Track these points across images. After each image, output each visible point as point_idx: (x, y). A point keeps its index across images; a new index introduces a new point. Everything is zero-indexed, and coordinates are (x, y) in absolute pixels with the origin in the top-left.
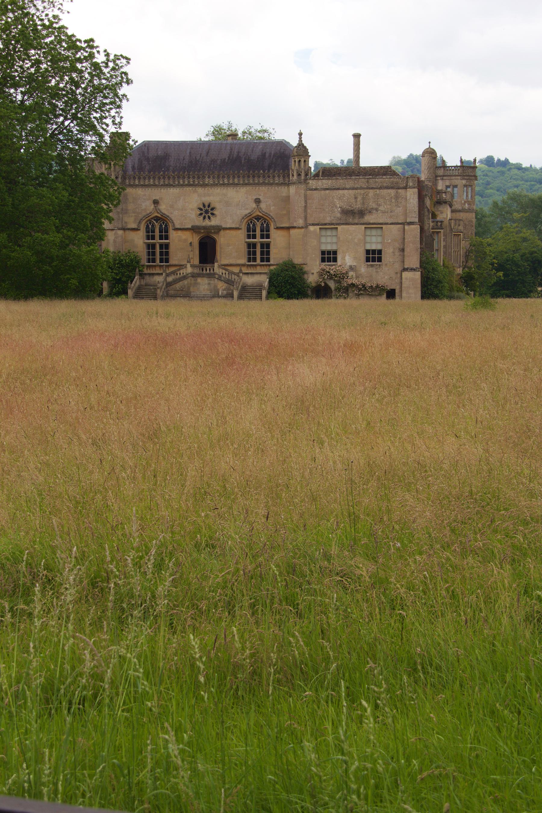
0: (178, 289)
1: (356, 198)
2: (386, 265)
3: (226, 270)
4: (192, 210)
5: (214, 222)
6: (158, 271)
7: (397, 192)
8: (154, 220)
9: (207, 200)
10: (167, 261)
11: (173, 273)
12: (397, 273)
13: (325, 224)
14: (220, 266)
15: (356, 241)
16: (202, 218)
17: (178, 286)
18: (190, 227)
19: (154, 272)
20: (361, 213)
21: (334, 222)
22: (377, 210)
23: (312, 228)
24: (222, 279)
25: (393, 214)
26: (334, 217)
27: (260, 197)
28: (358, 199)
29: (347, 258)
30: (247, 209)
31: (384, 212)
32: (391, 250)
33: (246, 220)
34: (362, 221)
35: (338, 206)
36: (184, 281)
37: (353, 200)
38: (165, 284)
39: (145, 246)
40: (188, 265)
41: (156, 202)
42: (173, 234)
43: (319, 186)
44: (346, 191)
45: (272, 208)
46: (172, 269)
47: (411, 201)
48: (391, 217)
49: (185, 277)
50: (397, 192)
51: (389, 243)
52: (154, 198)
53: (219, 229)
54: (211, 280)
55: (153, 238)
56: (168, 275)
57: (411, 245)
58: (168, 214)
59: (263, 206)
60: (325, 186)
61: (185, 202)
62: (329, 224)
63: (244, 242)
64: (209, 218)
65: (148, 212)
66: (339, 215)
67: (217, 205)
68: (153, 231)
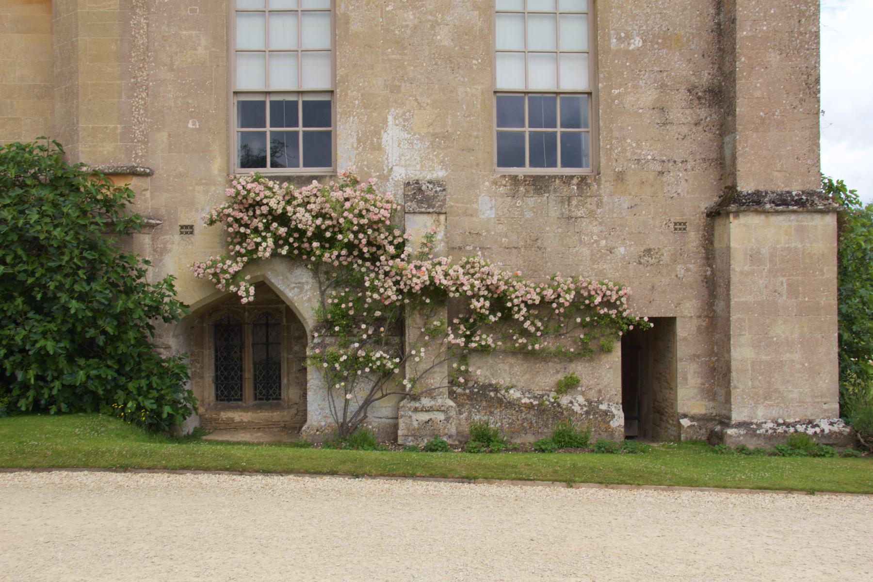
2: (620, 177)
12: (680, 227)
15: (444, 37)
32: (648, 96)
51: (634, 56)
57: (773, 57)
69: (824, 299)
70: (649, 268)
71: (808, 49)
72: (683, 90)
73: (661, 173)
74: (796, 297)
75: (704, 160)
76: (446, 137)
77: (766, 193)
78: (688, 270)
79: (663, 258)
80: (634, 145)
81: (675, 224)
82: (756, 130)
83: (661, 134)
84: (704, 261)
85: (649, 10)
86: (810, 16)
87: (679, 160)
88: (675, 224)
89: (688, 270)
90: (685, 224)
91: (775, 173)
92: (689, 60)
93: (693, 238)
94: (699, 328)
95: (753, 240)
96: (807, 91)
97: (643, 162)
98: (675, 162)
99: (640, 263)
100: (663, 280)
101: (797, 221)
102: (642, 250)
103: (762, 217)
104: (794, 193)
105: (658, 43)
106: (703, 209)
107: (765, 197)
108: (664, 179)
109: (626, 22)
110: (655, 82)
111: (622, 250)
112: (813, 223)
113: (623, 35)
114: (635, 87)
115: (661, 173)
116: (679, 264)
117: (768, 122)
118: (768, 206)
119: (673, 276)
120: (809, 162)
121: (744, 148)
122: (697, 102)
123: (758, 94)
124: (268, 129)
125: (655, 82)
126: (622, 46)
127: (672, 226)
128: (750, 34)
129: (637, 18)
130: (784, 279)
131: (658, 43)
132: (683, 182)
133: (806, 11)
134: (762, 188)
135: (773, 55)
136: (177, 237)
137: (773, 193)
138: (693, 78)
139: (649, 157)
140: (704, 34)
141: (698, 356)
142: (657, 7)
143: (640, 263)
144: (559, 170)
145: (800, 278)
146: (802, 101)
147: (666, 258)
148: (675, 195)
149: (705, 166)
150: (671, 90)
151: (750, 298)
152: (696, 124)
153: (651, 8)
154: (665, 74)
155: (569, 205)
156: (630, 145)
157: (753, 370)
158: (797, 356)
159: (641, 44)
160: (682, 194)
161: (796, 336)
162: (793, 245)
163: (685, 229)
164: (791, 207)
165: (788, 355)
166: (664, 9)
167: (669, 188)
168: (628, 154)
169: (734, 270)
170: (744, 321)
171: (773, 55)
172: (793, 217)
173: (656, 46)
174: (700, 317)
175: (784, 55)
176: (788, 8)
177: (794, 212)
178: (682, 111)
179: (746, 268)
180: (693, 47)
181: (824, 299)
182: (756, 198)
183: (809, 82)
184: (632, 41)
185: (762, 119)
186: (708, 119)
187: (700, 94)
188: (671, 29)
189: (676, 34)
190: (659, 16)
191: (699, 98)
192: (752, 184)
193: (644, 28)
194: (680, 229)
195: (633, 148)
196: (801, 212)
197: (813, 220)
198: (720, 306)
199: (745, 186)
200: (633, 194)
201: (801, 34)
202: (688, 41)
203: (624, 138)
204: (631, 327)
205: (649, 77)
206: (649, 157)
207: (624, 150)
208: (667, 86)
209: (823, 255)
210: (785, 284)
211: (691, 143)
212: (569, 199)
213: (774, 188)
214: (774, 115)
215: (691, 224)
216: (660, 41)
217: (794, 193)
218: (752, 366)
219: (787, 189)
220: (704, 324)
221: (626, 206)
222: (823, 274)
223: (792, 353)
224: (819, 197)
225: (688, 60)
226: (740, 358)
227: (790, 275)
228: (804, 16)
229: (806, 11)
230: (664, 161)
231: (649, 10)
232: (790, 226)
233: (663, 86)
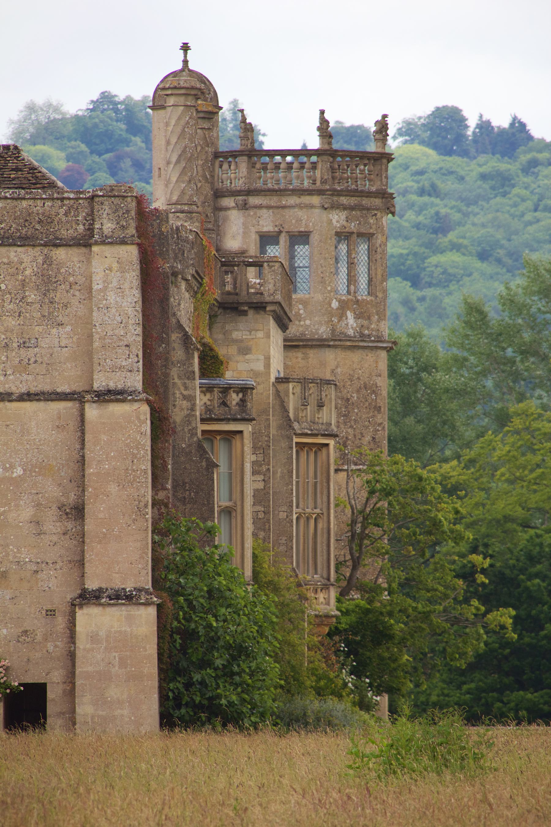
7: (48, 261)
12: (51, 613)
25: (31, 352)
47: (112, 297)
50: (48, 261)
57: (113, 488)
69: (146, 669)
70: (25, 645)
71: (139, 482)
72: (54, 507)
73: (36, 572)
74: (126, 668)
75: (70, 562)
77: (107, 589)
78: (56, 646)
79: (36, 637)
80: (15, 550)
81: (47, 611)
82: (100, 542)
83: (36, 542)
84: (69, 640)
85: (28, 446)
86: (141, 458)
87: (50, 562)
88: (47, 611)
89: (56, 646)
90: (54, 611)
91: (114, 575)
92: (60, 485)
93: (61, 622)
94: (64, 691)
95: (94, 625)
96: (138, 513)
97: (22, 563)
98: (47, 563)
99: (19, 641)
100: (37, 654)
101: (127, 611)
102: (21, 631)
103: (101, 608)
104: (127, 590)
105: (35, 472)
106: (68, 600)
107: (104, 593)
108: (39, 577)
109: (11, 456)
110: (33, 501)
112: (139, 613)
113: (8, 466)
114: (17, 506)
115: (36, 572)
116: (49, 642)
117: (108, 536)
118: (103, 600)
119: (44, 651)
120: (140, 566)
121: (90, 555)
122: (65, 517)
123: (101, 516)
125: (33, 501)
126: (7, 474)
127: (44, 612)
128: (96, 471)
129: (20, 452)
130: (116, 654)
131: (35, 472)
132: (53, 578)
133: (137, 454)
134: (104, 586)
135: (113, 487)
137: (111, 589)
138: (62, 498)
139: (27, 560)
140: (72, 464)
141: (63, 714)
142: (34, 444)
143: (19, 641)
145: (128, 653)
146: (134, 520)
147: (39, 638)
148: (47, 589)
149: (70, 566)
150: (45, 508)
151: (90, 669)
152: (64, 534)
153: (30, 445)
154: (40, 495)
155: (164, 800)
156: (12, 550)
157: (93, 722)
158: (125, 712)
159: (22, 472)
160: (52, 588)
161: (125, 696)
162: (123, 629)
163: (54, 615)
164: (120, 601)
165: (119, 711)
166: (41, 445)
167: (42, 583)
168: (11, 558)
169: (79, 648)
170: (86, 686)
171: (113, 487)
172: (124, 608)
173: (34, 474)
174: (65, 683)
175: (121, 486)
176: (124, 452)
177: (123, 604)
178: (53, 524)
179: (88, 646)
180: (63, 474)
181: (146, 669)
182: (97, 594)
183: (140, 506)
184: (15, 470)
185: (105, 534)
186: (74, 530)
187: (68, 510)
188: (46, 461)
189: (49, 465)
190: (36, 450)
191: (67, 514)
192: (96, 583)
193: (25, 460)
194: (51, 615)
195: (14, 552)
196: (129, 604)
197: (138, 610)
199: (92, 585)
200: (14, 588)
201: (134, 471)
202: (59, 469)
203: (8, 545)
204: (8, 691)
205: (28, 498)
206: (27, 560)
207: (7, 555)
208: (42, 504)
209: (146, 636)
210: (117, 658)
211: (60, 548)
213: (113, 586)
214: (113, 531)
215: (59, 611)
216: (37, 470)
217: (127, 590)
218: (92, 719)
219: (123, 586)
220: (68, 688)
221: (8, 597)
222: (146, 650)
223: (122, 709)
224: (146, 593)
225: (58, 485)
226: (83, 713)
227: (121, 651)
228: (136, 457)
229: (137, 454)
230: (38, 563)
231: (28, 446)
232: (121, 615)
233: (38, 505)
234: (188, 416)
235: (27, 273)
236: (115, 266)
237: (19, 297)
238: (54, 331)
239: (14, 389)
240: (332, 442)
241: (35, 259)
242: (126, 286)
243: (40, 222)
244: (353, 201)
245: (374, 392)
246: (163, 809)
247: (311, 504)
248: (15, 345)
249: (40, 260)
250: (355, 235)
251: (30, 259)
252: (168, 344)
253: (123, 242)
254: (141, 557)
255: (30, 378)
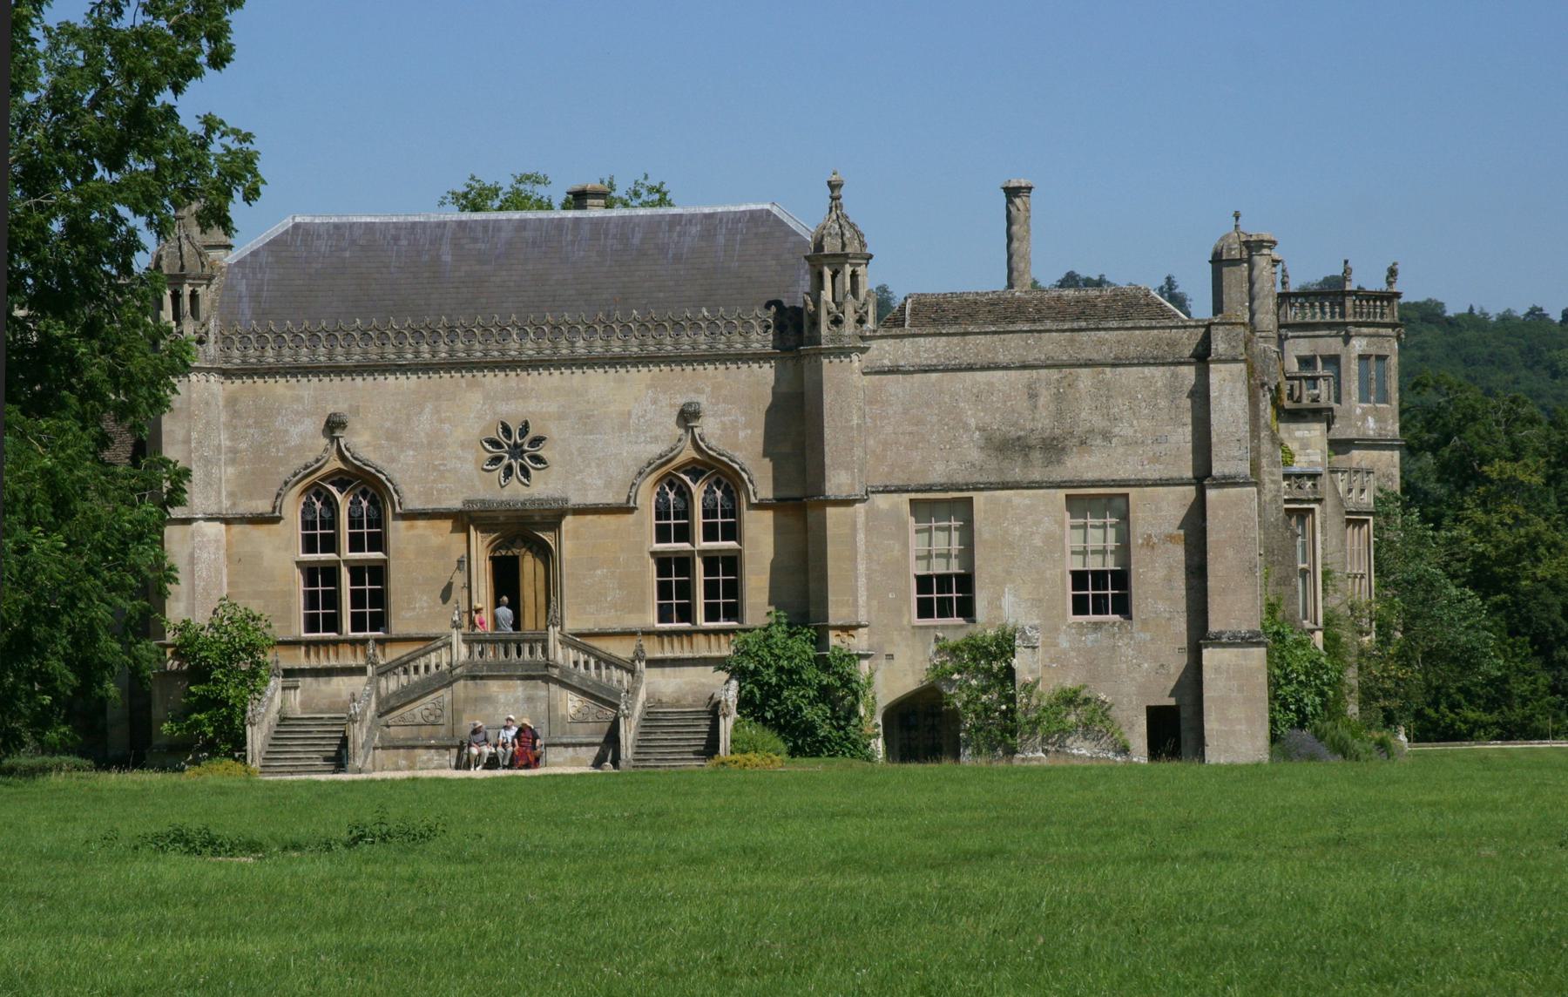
0: (419, 719)
1: (1033, 396)
3: (589, 651)
4: (463, 445)
5: (543, 487)
6: (348, 658)
7: (1175, 376)
8: (333, 484)
9: (513, 411)
10: (379, 622)
11: (403, 665)
13: (930, 489)
14: (569, 641)
15: (1038, 541)
16: (499, 471)
17: (419, 709)
18: (456, 504)
19: (333, 662)
20: (1054, 447)
21: (959, 479)
22: (1106, 436)
23: (882, 502)
24: (575, 681)
25: (1162, 448)
26: (960, 464)
27: (703, 400)
28: (1042, 401)
29: (1008, 600)
30: (655, 439)
31: (1130, 443)
33: (654, 477)
34: (1057, 474)
35: (972, 422)
36: (441, 692)
37: (1023, 404)
38: (373, 705)
39: (299, 577)
40: (456, 637)
41: (333, 426)
42: (398, 531)
43: (904, 356)
44: (1000, 373)
45: (742, 434)
46: (395, 653)
47: (1226, 402)
48: (1156, 459)
49: (446, 679)
50: (1175, 376)
52: (331, 409)
53: (554, 516)
54: (536, 687)
55: (330, 544)
56: (384, 672)
57: (1230, 553)
58: (379, 463)
59: (710, 428)
60: (925, 359)
61: (441, 421)
62: (945, 489)
63: (647, 556)
64: (525, 471)
65: (311, 457)
66: (975, 455)
67: (552, 430)
68: (686, 513)
76: (1040, 600)
82: (1219, 595)
111: (1146, 665)
115: (1169, 619)
124: (365, 530)
130: (1235, 683)
136: (884, 661)
144: (368, 634)
149: (1009, 630)
198: (1131, 483)
212: (1114, 635)
213: (1231, 629)
234: (1276, 496)
235: (1159, 384)
236: (1228, 377)
237: (1152, 404)
238: (1180, 430)
239: (1149, 476)
240: (1371, 518)
241: (1164, 375)
242: (1237, 393)
243: (1168, 345)
244: (1371, 330)
245: (1391, 480)
246: (40, 896)
247: (1356, 567)
248: (1150, 442)
249: (1168, 375)
250: (1373, 359)
251: (1160, 374)
252: (1259, 440)
253: (1235, 360)
254: (1253, 606)
255: (1161, 467)
